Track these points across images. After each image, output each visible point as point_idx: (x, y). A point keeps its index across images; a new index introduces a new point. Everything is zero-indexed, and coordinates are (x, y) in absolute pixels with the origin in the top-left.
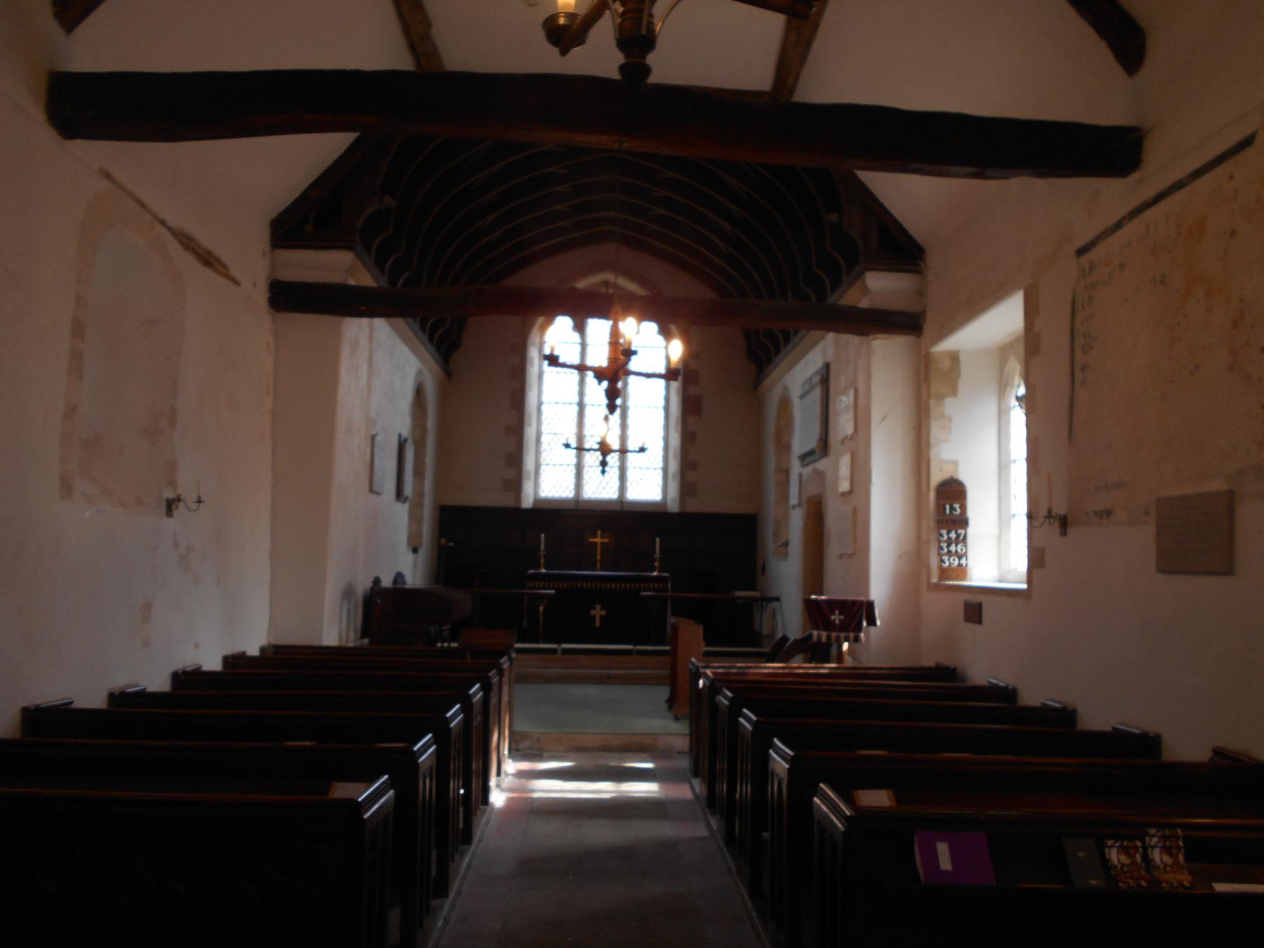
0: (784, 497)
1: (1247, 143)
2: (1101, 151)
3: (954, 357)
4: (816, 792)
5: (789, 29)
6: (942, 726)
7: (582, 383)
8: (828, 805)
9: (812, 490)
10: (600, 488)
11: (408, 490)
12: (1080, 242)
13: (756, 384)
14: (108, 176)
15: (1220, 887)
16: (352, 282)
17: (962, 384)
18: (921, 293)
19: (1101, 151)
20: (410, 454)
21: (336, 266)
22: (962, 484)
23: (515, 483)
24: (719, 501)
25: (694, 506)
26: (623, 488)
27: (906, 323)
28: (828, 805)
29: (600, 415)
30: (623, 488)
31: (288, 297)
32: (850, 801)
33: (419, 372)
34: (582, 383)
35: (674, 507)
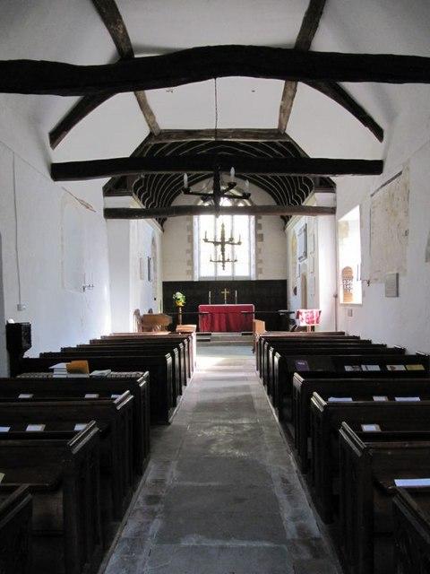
0: (295, 273)
1: (400, 173)
2: (374, 167)
3: (347, 223)
4: (312, 395)
5: (309, 43)
6: (338, 358)
7: (216, 267)
8: (317, 400)
9: (303, 271)
10: (225, 273)
11: (152, 278)
12: (372, 193)
13: (284, 229)
14: (64, 189)
15: (418, 399)
16: (132, 207)
17: (350, 234)
18: (335, 200)
19: (374, 167)
20: (152, 263)
21: (130, 202)
22: (338, 271)
23: (191, 272)
24: (271, 275)
25: (261, 277)
26: (233, 271)
27: (332, 211)
28: (317, 400)
29: (224, 243)
30: (233, 271)
31: (111, 213)
32: (326, 400)
33: (153, 232)
34: (216, 267)
35: (254, 278)
